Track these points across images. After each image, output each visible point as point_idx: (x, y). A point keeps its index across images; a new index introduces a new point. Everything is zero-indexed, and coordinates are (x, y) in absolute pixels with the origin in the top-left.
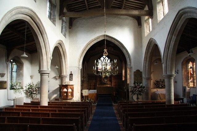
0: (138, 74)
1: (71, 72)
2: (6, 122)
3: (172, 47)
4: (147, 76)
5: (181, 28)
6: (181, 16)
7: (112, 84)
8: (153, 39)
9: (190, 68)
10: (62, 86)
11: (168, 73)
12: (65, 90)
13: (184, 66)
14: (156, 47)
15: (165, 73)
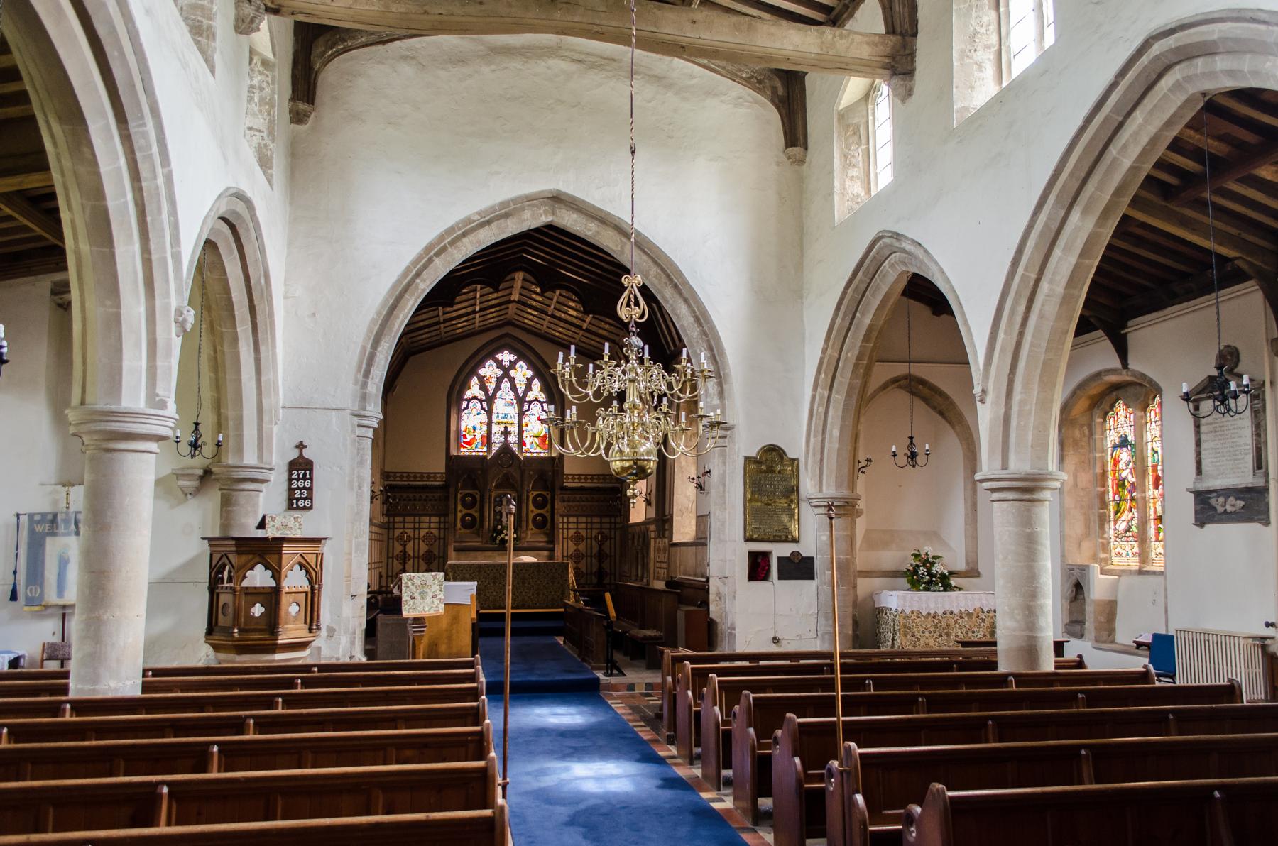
0: (770, 474)
1: (301, 446)
2: (68, 713)
3: (1060, 290)
4: (830, 490)
5: (1136, 161)
6: (1160, 76)
7: (552, 550)
8: (898, 236)
9: (1115, 447)
10: (239, 552)
11: (1020, 465)
12: (259, 577)
13: (1077, 433)
14: (925, 295)
15: (998, 463)
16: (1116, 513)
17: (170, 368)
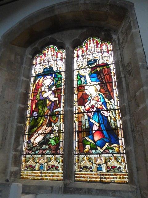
16: (31, 128)
17: (118, 185)
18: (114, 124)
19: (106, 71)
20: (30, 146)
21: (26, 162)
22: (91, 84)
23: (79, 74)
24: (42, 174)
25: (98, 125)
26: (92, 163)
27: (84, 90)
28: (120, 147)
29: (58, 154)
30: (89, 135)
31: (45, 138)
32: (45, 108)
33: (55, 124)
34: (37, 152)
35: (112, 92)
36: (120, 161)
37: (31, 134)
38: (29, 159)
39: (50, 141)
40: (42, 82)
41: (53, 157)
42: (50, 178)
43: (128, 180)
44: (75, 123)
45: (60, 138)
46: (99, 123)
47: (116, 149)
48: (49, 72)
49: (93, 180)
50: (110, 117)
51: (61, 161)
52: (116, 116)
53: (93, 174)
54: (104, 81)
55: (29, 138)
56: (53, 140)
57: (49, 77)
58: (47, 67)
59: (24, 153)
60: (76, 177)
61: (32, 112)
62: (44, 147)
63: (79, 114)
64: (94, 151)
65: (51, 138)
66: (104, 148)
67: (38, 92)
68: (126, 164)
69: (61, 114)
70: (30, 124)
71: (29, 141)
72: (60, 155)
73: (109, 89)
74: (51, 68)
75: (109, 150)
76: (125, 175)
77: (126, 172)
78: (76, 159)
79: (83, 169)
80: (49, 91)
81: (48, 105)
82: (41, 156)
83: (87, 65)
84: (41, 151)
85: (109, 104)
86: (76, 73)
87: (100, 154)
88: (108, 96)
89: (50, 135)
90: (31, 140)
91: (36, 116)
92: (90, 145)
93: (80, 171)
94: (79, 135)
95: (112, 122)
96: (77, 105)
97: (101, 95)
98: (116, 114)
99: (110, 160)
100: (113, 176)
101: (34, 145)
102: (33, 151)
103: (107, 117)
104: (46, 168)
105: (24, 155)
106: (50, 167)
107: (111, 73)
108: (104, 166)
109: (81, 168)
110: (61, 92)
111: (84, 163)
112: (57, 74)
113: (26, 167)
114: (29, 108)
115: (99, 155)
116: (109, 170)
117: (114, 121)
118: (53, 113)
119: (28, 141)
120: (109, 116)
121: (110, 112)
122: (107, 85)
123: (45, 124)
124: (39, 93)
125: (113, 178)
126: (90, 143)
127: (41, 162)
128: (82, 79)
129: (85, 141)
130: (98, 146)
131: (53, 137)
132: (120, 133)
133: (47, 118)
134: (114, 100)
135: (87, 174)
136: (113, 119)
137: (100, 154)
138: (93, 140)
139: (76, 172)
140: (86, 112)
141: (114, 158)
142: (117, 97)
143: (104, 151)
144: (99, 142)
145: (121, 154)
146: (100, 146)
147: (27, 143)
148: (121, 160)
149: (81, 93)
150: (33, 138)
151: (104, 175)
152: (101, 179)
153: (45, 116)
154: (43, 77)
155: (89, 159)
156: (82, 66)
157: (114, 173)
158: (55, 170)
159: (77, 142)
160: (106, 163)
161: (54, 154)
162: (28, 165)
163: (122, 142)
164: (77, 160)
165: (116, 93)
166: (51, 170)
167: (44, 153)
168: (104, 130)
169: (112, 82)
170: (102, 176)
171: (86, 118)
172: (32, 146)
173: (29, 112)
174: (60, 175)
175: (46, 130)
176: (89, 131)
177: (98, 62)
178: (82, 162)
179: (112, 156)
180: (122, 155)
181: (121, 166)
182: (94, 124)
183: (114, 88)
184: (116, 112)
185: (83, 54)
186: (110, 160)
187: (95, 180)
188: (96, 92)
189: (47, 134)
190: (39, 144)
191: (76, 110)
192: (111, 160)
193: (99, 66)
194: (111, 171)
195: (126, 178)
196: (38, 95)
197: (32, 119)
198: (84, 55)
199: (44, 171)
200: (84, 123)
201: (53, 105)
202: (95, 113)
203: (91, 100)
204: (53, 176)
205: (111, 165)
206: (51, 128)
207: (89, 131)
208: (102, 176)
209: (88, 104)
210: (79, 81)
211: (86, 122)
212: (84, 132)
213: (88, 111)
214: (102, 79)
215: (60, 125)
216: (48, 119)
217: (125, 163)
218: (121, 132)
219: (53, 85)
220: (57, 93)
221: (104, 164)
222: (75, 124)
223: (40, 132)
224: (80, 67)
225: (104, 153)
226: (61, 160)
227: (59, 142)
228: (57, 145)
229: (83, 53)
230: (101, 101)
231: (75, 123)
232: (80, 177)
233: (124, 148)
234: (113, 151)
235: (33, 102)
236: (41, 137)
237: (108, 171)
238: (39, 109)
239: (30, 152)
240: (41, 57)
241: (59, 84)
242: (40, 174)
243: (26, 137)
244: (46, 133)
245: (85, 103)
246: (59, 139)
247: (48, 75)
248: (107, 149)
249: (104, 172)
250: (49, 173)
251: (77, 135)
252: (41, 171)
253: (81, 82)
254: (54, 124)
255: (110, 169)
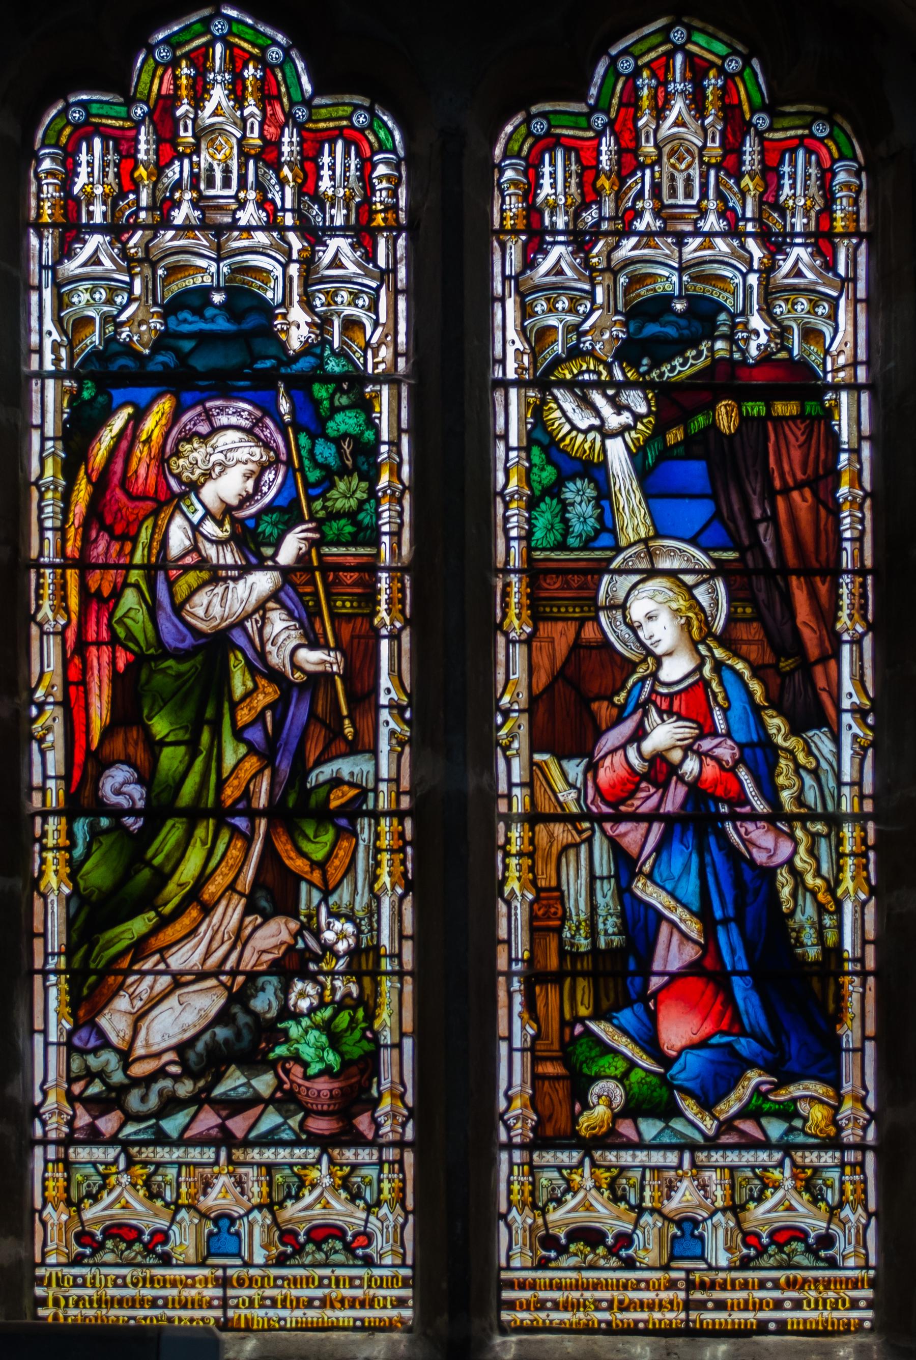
16: (93, 915)
18: (820, 930)
19: (796, 454)
20: (101, 1074)
21: (74, 1205)
22: (651, 555)
23: (540, 437)
24: (231, 1292)
25: (693, 928)
26: (167, 1205)
27: (590, 607)
28: (840, 1099)
29: (359, 1141)
30: (626, 1002)
31: (236, 1009)
32: (217, 734)
33: (325, 899)
34: (172, 1125)
35: (823, 659)
36: (831, 1197)
37: (103, 974)
38: (105, 1177)
39: (288, 1040)
40: (162, 460)
41: (319, 1161)
42: (298, 1313)
43: (869, 1314)
44: (508, 903)
45: (371, 1017)
46: (704, 914)
47: (818, 1113)
48: (220, 352)
49: (636, 1322)
50: (797, 875)
51: (386, 1195)
52: (840, 869)
53: (639, 1281)
54: (770, 554)
55: (87, 1002)
56: (317, 1027)
57: (238, 412)
58: (205, 292)
59: (56, 1128)
60: (511, 1305)
61: (84, 768)
62: (233, 1082)
63: (540, 828)
64: (650, 1129)
65: (296, 1016)
66: (730, 1106)
67: (130, 567)
68: (869, 1215)
69: (376, 815)
70: (72, 877)
71: (84, 1033)
72: (381, 1147)
73: (807, 633)
74: (246, 303)
75: (764, 1121)
76: (856, 1284)
77: (867, 1267)
78: (510, 1183)
79: (563, 1250)
80: (245, 570)
81: (244, 716)
82: (209, 1154)
83: (627, 353)
84: (208, 1120)
85: (798, 767)
86: (511, 415)
87: (693, 1147)
88: (788, 698)
89: (286, 989)
90: (103, 1022)
91: (132, 812)
92: (622, 1079)
93: (543, 1264)
94: (540, 1004)
95: (807, 913)
96: (521, 744)
97: (739, 675)
98: (841, 855)
99: (762, 1192)
100: (777, 1294)
101: (138, 1070)
102: (130, 1117)
103: (769, 873)
104: (265, 1247)
105: (51, 1149)
106: (302, 1239)
107: (837, 476)
108: (721, 1232)
109: (549, 1241)
110: (370, 597)
111: (574, 1210)
112: (321, 391)
113: (83, 1237)
114: (50, 723)
115: (687, 1156)
116: (753, 1252)
117: (821, 909)
118: (306, 794)
119: (71, 1034)
120: (790, 862)
121: (799, 833)
122: (788, 585)
123: (232, 887)
124: (135, 576)
125: (778, 1305)
126: (621, 1066)
127: (214, 1200)
128: (570, 492)
129: (582, 1050)
130: (687, 1092)
131: (312, 1010)
132: (853, 1003)
133: (249, 840)
134: (836, 740)
135: (596, 1286)
136: (814, 894)
137: (693, 1147)
138: (650, 1042)
139: (509, 1268)
140: (601, 818)
141: (794, 1177)
142: (859, 712)
143: (727, 1126)
144: (693, 1062)
145: (843, 1147)
146: (702, 1087)
147: (532, 1049)
148: (842, 1192)
149: (561, 636)
150: (122, 1003)
151: (712, 1286)
152: (693, 1315)
153: (221, 815)
154: (165, 405)
155: (614, 1180)
156: (575, 353)
157: (782, 1275)
158: (340, 1258)
159: (517, 1056)
160: (736, 1209)
161: (324, 1143)
162: (97, 1221)
163: (861, 1071)
164: (516, 1187)
165: (851, 679)
166: (308, 1260)
167: (240, 1134)
168: (741, 974)
169: (836, 571)
170: (698, 1295)
171: (603, 863)
172: (118, 1077)
173: (55, 761)
174: (381, 1292)
175: (240, 939)
176: (620, 972)
177: (730, 338)
178: (560, 1202)
179: (781, 1165)
180: (851, 1156)
181: (835, 1228)
182: (660, 917)
183: (846, 621)
184: (840, 842)
185: (590, 216)
186: (765, 1186)
187: (646, 1322)
188: (695, 644)
189: (252, 976)
190: (183, 1062)
191: (516, 791)
192: (768, 1192)
193: (725, 379)
194: (764, 1261)
195: (862, 1304)
196: (130, 598)
197: (95, 833)
198: (596, 233)
199: (247, 1265)
200: (582, 905)
201: (298, 713)
202: (678, 829)
203: (646, 714)
204: (325, 1302)
205: (769, 1222)
206: (294, 925)
207: (620, 972)
208: (698, 1295)
209: (623, 747)
210: (548, 506)
211: (600, 899)
212: (582, 983)
213: (616, 804)
214: (752, 525)
215: (374, 912)
216: (257, 847)
217: (403, 1207)
218: (859, 1001)
219: (287, 513)
220: (323, 594)
221: (719, 1216)
222: (502, 908)
223: (185, 957)
224: (558, 362)
225: (725, 1139)
226: (386, 1186)
227: (367, 1046)
228: (354, 1070)
229: (585, 206)
230: (729, 735)
231: (508, 903)
232: (541, 1305)
233: (867, 1110)
234: (791, 1130)
235: (85, 662)
236: (202, 1004)
237: (745, 1264)
238: (154, 746)
239: (107, 1124)
240: (123, 144)
241: (351, 515)
242: (219, 1292)
243: (51, 1004)
244: (248, 962)
245: (599, 734)
246: (370, 1027)
247: (224, 385)
248: (749, 1113)
249: (718, 1269)
250: (295, 1282)
251: (518, 999)
252: (225, 1267)
253: (565, 521)
254: (316, 896)
255: (753, 1248)
